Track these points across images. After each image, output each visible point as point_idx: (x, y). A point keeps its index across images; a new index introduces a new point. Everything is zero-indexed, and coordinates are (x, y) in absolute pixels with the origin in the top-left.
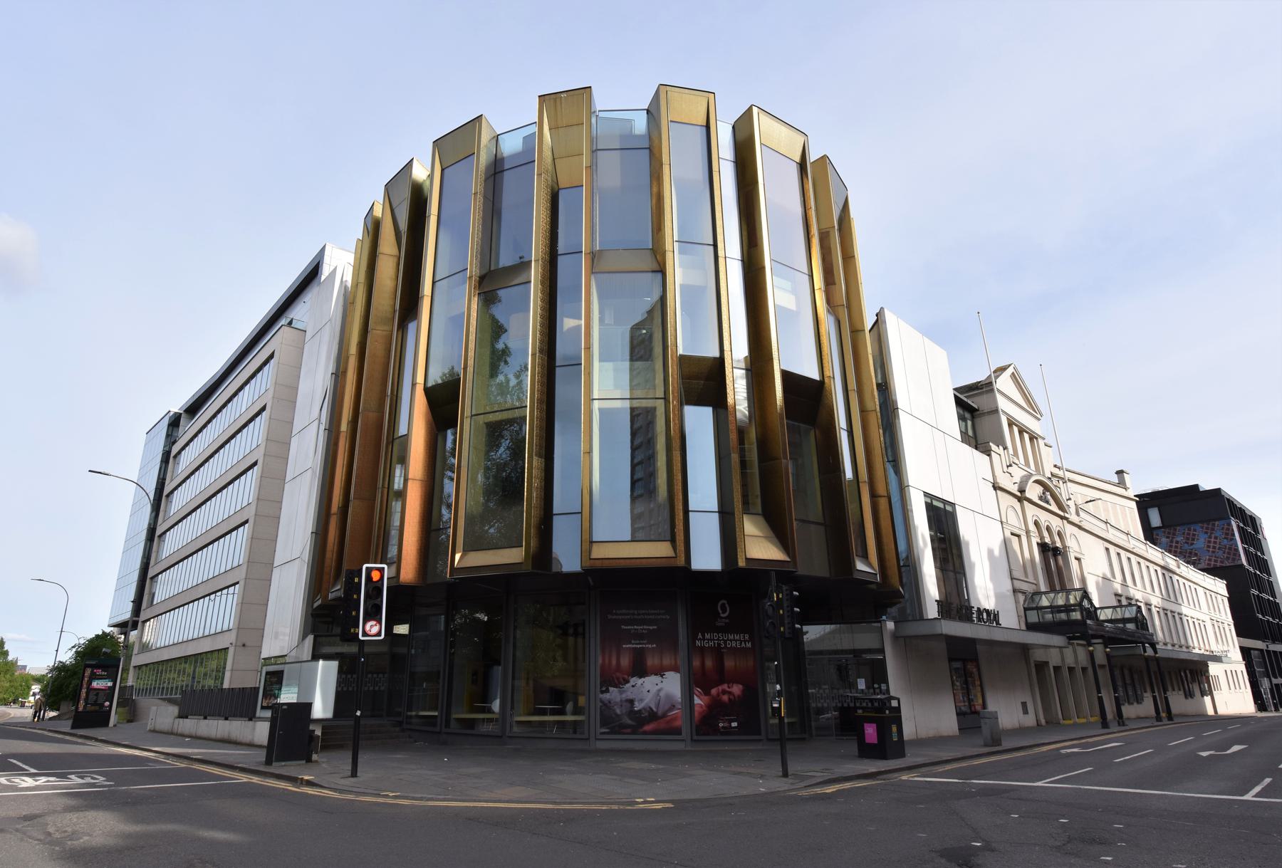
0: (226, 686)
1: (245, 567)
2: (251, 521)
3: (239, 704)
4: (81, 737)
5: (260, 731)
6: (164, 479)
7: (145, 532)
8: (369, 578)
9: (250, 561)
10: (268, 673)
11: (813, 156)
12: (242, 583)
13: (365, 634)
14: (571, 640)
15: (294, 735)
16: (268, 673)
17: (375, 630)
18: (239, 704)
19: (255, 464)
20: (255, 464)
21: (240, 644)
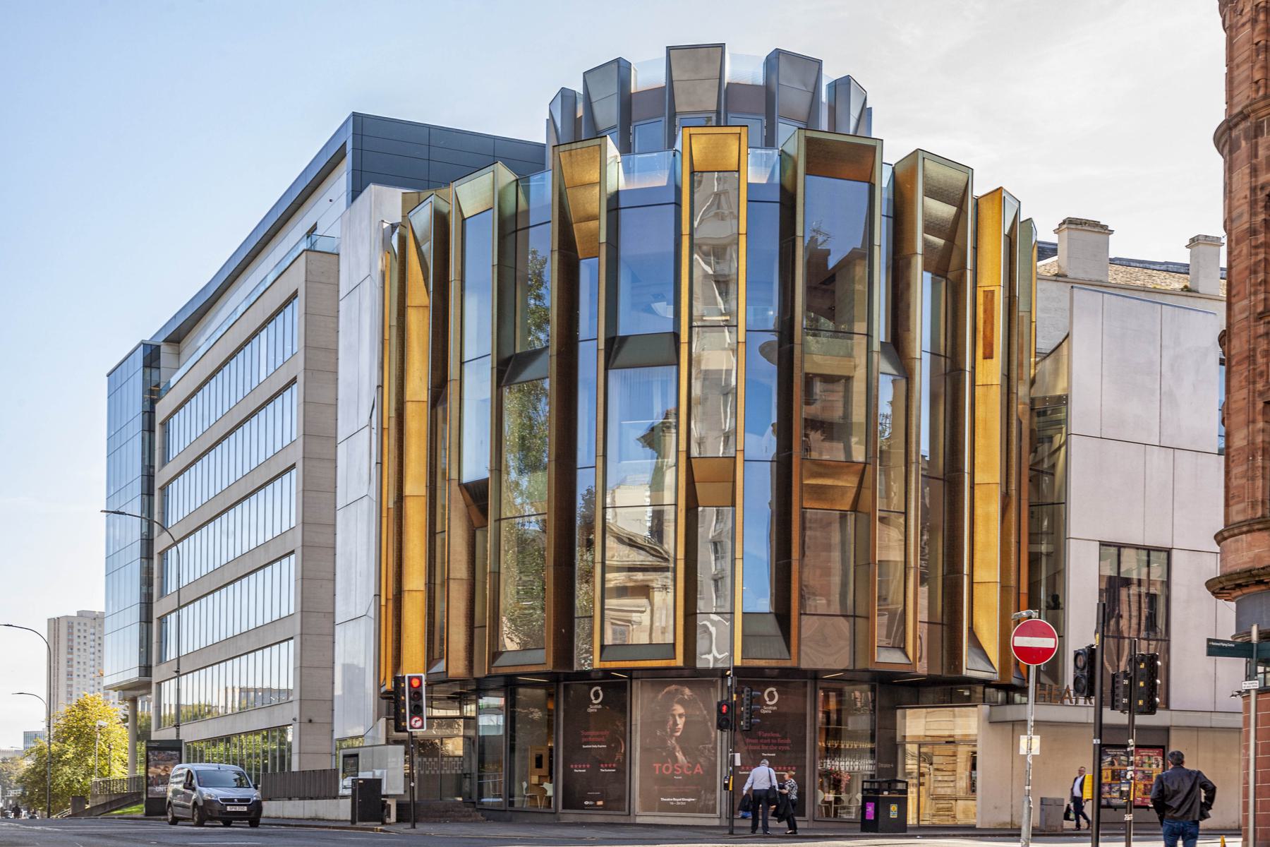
0: (295, 768)
1: (298, 617)
2: (301, 379)
3: (318, 784)
4: (442, 644)
5: (342, 809)
6: (151, 466)
7: (137, 546)
8: (411, 685)
9: (304, 611)
10: (345, 756)
11: (1023, 218)
12: (300, 465)
13: (411, 727)
14: (196, 703)
15: (369, 800)
16: (345, 756)
17: (419, 724)
18: (318, 784)
19: (295, 295)
20: (295, 295)
21: (305, 720)
